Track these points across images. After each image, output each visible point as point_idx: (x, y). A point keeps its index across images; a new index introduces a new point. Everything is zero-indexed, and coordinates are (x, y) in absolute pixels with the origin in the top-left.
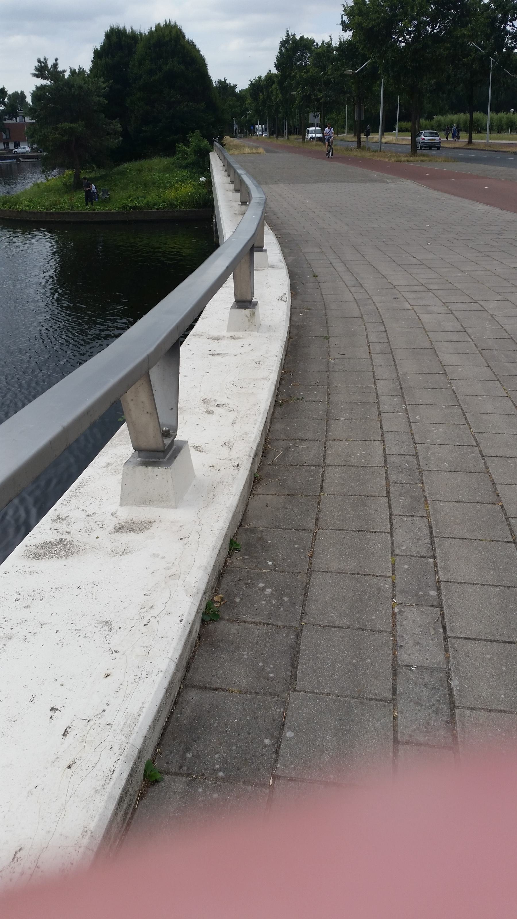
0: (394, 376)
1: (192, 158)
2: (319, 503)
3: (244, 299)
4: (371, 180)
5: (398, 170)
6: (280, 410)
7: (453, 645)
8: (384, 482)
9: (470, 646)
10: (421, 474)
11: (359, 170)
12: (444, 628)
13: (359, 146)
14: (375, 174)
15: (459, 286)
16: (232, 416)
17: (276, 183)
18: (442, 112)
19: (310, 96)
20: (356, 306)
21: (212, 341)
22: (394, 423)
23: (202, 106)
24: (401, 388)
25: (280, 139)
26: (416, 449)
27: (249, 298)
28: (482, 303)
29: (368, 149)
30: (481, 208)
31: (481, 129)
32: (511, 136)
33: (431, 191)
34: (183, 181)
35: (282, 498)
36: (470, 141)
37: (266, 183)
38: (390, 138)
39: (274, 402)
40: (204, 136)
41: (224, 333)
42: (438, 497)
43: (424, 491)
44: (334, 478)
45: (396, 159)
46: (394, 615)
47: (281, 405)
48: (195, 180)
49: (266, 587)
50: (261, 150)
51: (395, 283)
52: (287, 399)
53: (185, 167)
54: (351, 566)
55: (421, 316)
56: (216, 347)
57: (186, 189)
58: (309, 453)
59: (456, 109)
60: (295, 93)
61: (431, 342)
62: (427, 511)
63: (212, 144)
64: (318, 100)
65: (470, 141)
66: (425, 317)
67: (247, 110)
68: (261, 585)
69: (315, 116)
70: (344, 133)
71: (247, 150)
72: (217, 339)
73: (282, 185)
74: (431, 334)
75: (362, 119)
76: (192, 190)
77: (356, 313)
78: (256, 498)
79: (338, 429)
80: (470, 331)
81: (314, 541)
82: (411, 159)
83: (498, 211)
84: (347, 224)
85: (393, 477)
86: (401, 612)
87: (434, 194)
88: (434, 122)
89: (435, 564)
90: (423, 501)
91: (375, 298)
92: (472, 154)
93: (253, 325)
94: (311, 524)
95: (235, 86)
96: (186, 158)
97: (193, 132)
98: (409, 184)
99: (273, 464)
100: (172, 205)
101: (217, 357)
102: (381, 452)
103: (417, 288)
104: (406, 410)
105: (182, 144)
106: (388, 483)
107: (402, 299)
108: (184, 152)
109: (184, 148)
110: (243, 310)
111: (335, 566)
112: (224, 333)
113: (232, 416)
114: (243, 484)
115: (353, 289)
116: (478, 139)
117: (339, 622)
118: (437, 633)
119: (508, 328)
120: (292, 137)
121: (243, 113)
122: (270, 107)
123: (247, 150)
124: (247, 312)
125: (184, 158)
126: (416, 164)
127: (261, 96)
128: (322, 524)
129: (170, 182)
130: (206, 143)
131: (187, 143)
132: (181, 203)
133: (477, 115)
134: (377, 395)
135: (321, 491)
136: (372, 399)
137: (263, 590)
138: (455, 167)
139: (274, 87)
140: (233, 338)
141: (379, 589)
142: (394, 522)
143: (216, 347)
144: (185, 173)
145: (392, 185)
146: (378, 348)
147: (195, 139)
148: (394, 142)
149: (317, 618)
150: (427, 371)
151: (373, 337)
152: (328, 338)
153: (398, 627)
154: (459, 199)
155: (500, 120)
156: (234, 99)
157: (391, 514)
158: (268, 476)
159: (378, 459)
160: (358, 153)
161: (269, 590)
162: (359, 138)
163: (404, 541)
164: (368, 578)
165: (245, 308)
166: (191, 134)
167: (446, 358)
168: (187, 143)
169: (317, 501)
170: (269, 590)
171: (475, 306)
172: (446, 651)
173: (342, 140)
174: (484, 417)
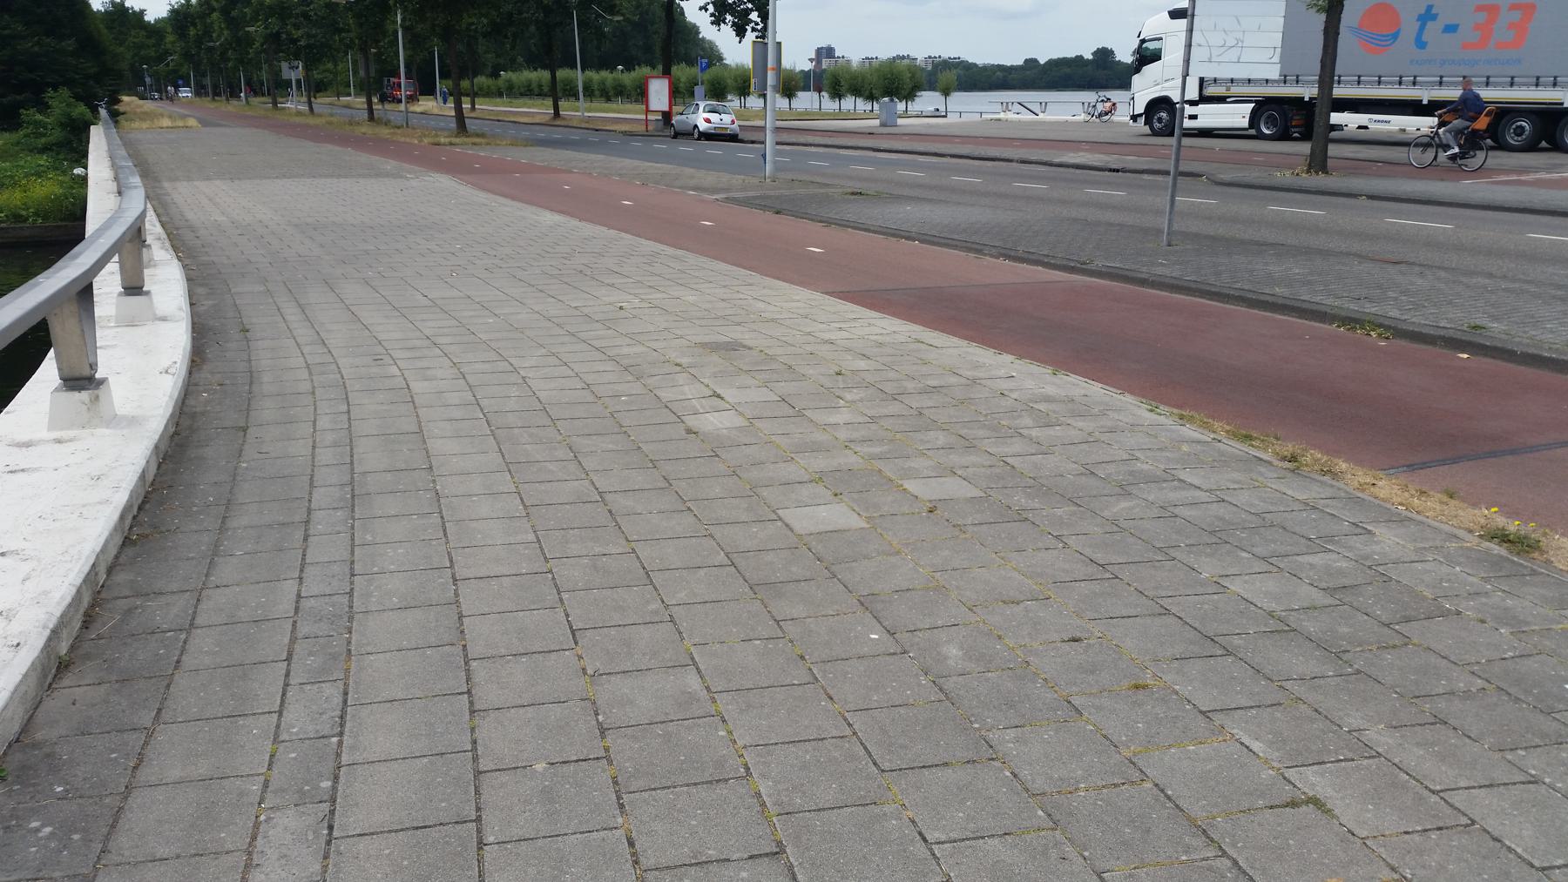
0: (347, 478)
1: (57, 135)
2: (168, 686)
3: (77, 374)
4: (379, 175)
5: (432, 160)
6: (130, 551)
7: (338, 847)
8: (286, 640)
9: (362, 844)
10: (351, 619)
11: (364, 158)
12: (331, 828)
13: (371, 117)
14: (390, 165)
15: (484, 337)
16: (26, 568)
17: (208, 179)
18: (512, 66)
19: (278, 35)
20: (306, 375)
21: (16, 449)
22: (327, 549)
23: (70, 44)
24: (353, 496)
25: (234, 102)
26: (352, 583)
27: (86, 372)
28: (512, 361)
29: (387, 123)
30: (548, 218)
31: (571, 93)
32: (621, 107)
33: (476, 192)
34: (38, 175)
35: (103, 689)
36: (557, 114)
37: (189, 179)
38: (427, 104)
39: (119, 540)
40: (78, 98)
41: (45, 434)
42: (369, 649)
43: (349, 643)
44: (203, 647)
45: (431, 140)
46: (257, 825)
47: (134, 543)
48: (64, 173)
49: (43, 826)
50: (192, 122)
51: (381, 337)
52: (147, 531)
53: (44, 150)
54: (203, 768)
55: (412, 385)
56: (20, 458)
57: (45, 189)
58: (166, 612)
59: (534, 62)
60: (252, 29)
61: (419, 423)
62: (347, 671)
63: (95, 110)
64: (294, 41)
65: (557, 114)
66: (417, 386)
67: (167, 53)
68: (34, 824)
69: (292, 68)
70: (349, 95)
71: (166, 122)
72: (27, 445)
73: (218, 182)
74: (421, 412)
75: (373, 74)
76: (59, 191)
77: (305, 386)
78: (56, 693)
79: (227, 570)
80: (484, 403)
81: (146, 743)
82: (457, 140)
83: (574, 222)
84: (322, 246)
85: (304, 629)
86: (268, 820)
87: (482, 197)
88: (500, 82)
89: (340, 743)
90: (342, 659)
91: (341, 362)
92: (557, 134)
93: (98, 416)
94: (146, 718)
95: (142, 12)
96: (44, 135)
97: (55, 90)
98: (444, 181)
99: (100, 637)
100: (18, 218)
101: (20, 475)
102: (293, 597)
103: (418, 343)
104: (353, 527)
105: (32, 111)
106: (293, 640)
107: (387, 360)
108: (37, 124)
109: (39, 117)
110: (76, 394)
111: (175, 773)
112: (45, 434)
113: (26, 568)
114: (24, 671)
115: (306, 350)
116: (568, 109)
117: (162, 852)
118: (317, 837)
119: (542, 395)
120: (255, 100)
121: (160, 59)
122: (210, 49)
123: (166, 122)
124: (84, 395)
125: (39, 135)
126: (464, 149)
127: (192, 32)
128: (165, 716)
129: (12, 177)
130: (81, 109)
131: (43, 107)
132: (36, 214)
133: (562, 74)
134: (309, 511)
135: (176, 668)
136: (300, 516)
137: (38, 830)
138: (525, 155)
139: (215, 15)
140: (59, 441)
141: (241, 794)
142: (289, 694)
143: (20, 458)
144: (43, 160)
145: (414, 183)
146: (329, 438)
147: (60, 102)
148: (436, 111)
149: (127, 853)
150: (403, 466)
151: (323, 423)
152: (245, 430)
153: (260, 841)
154: (520, 205)
155: (603, 82)
156: (143, 33)
157: (286, 685)
158: (88, 657)
159: (286, 606)
160: (367, 129)
161: (48, 830)
162: (370, 103)
163: (298, 720)
164: (225, 782)
165: (80, 389)
166: (50, 92)
167: (435, 445)
168: (43, 107)
169: (165, 683)
170: (48, 830)
171: (503, 366)
172: (326, 857)
173: (348, 107)
174: (474, 525)
